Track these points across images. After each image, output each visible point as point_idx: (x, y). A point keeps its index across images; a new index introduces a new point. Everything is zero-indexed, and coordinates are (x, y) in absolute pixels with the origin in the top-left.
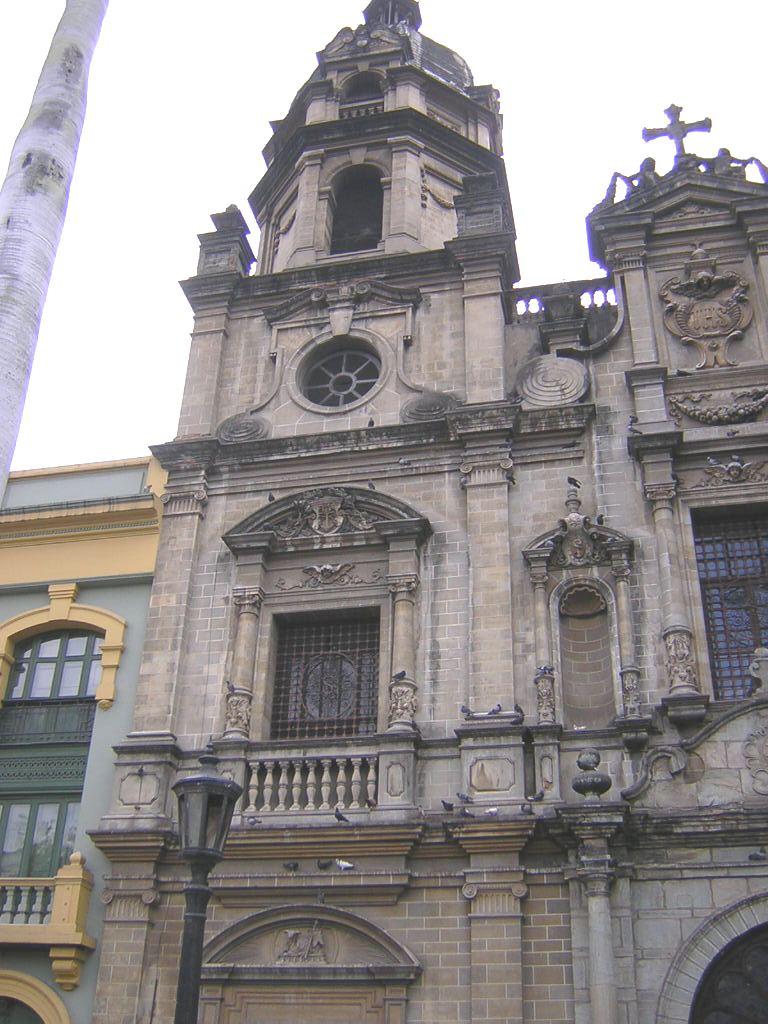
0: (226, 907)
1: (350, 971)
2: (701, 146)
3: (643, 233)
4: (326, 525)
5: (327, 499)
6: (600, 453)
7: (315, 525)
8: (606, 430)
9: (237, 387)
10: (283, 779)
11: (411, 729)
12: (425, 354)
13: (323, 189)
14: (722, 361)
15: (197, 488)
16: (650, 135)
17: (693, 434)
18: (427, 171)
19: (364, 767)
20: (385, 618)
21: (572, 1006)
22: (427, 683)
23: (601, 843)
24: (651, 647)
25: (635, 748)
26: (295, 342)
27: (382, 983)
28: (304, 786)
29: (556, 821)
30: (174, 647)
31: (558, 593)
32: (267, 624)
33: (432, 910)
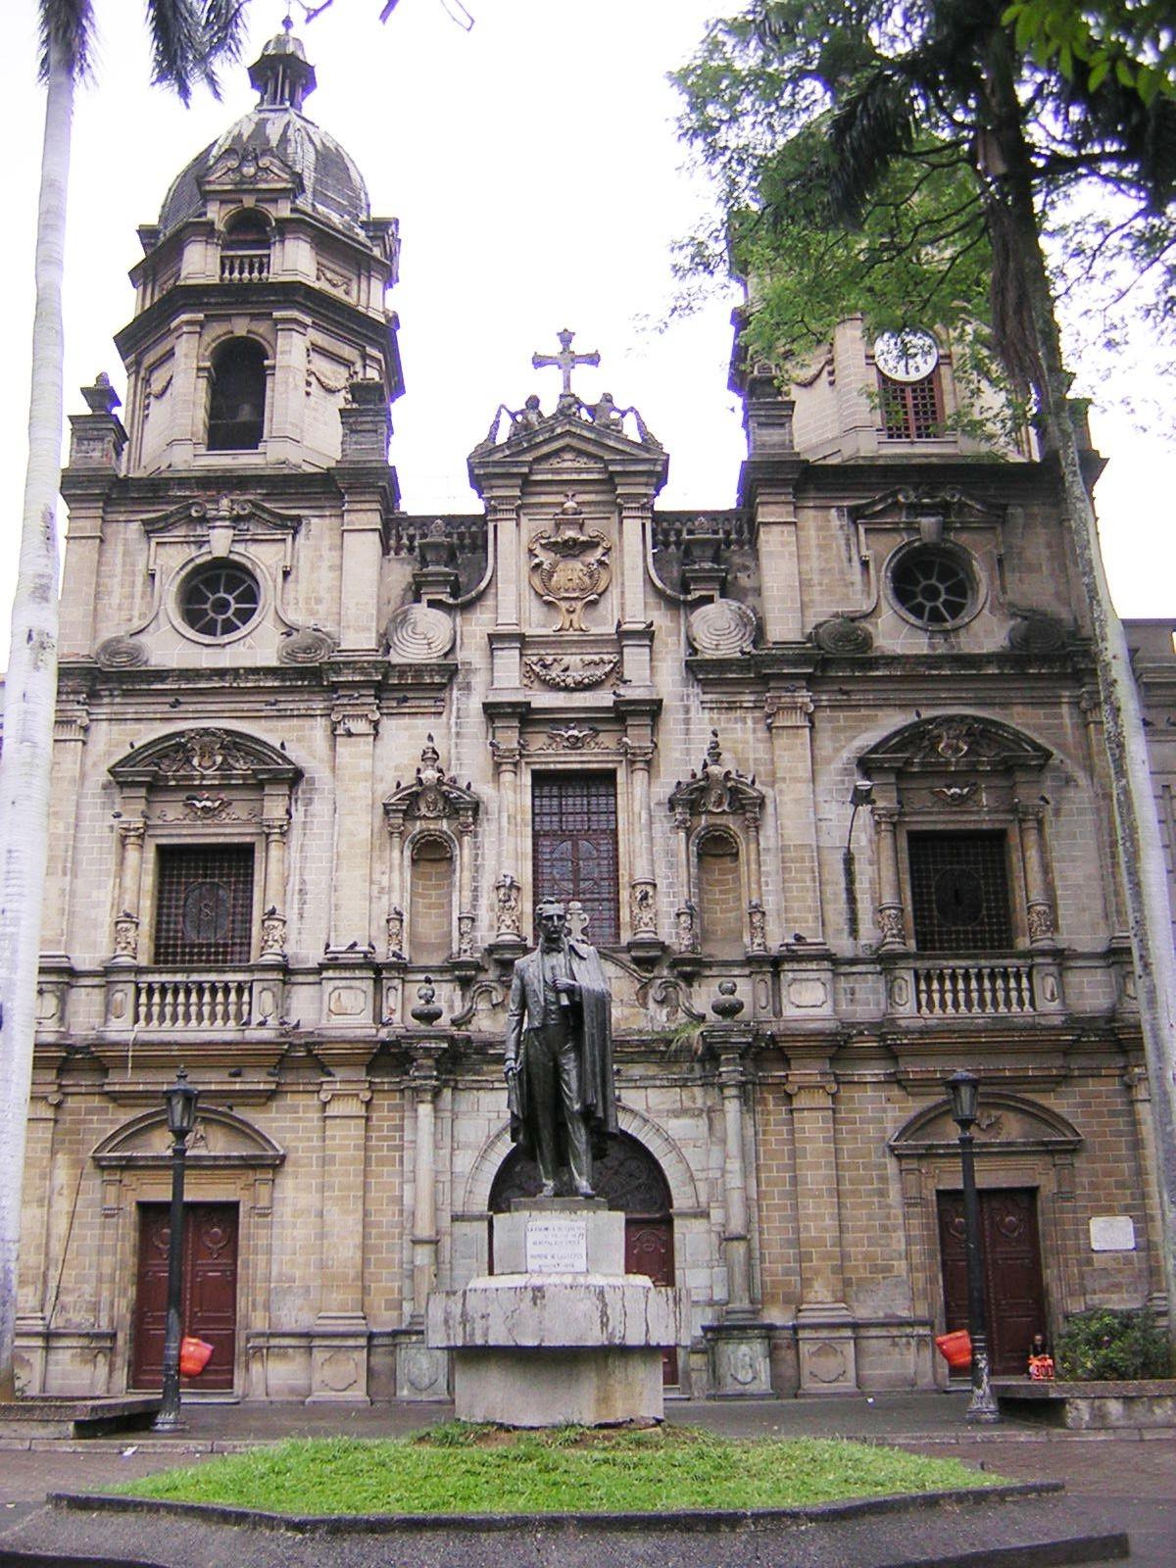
0: (120, 1106)
1: (228, 1158)
2: (588, 386)
3: (520, 482)
4: (206, 764)
5: (206, 739)
6: (458, 709)
7: (195, 762)
8: (467, 687)
9: (115, 600)
10: (169, 999)
11: (280, 958)
12: (303, 587)
13: (202, 364)
14: (576, 626)
15: (78, 714)
16: (539, 362)
17: (542, 699)
18: (316, 348)
19: (240, 990)
20: (259, 855)
21: (401, 1184)
22: (296, 917)
23: (430, 1062)
24: (485, 895)
25: (465, 983)
26: (174, 560)
27: (253, 1167)
28: (187, 1005)
29: (397, 1043)
30: (65, 874)
31: (411, 842)
32: (151, 854)
33: (294, 1109)
